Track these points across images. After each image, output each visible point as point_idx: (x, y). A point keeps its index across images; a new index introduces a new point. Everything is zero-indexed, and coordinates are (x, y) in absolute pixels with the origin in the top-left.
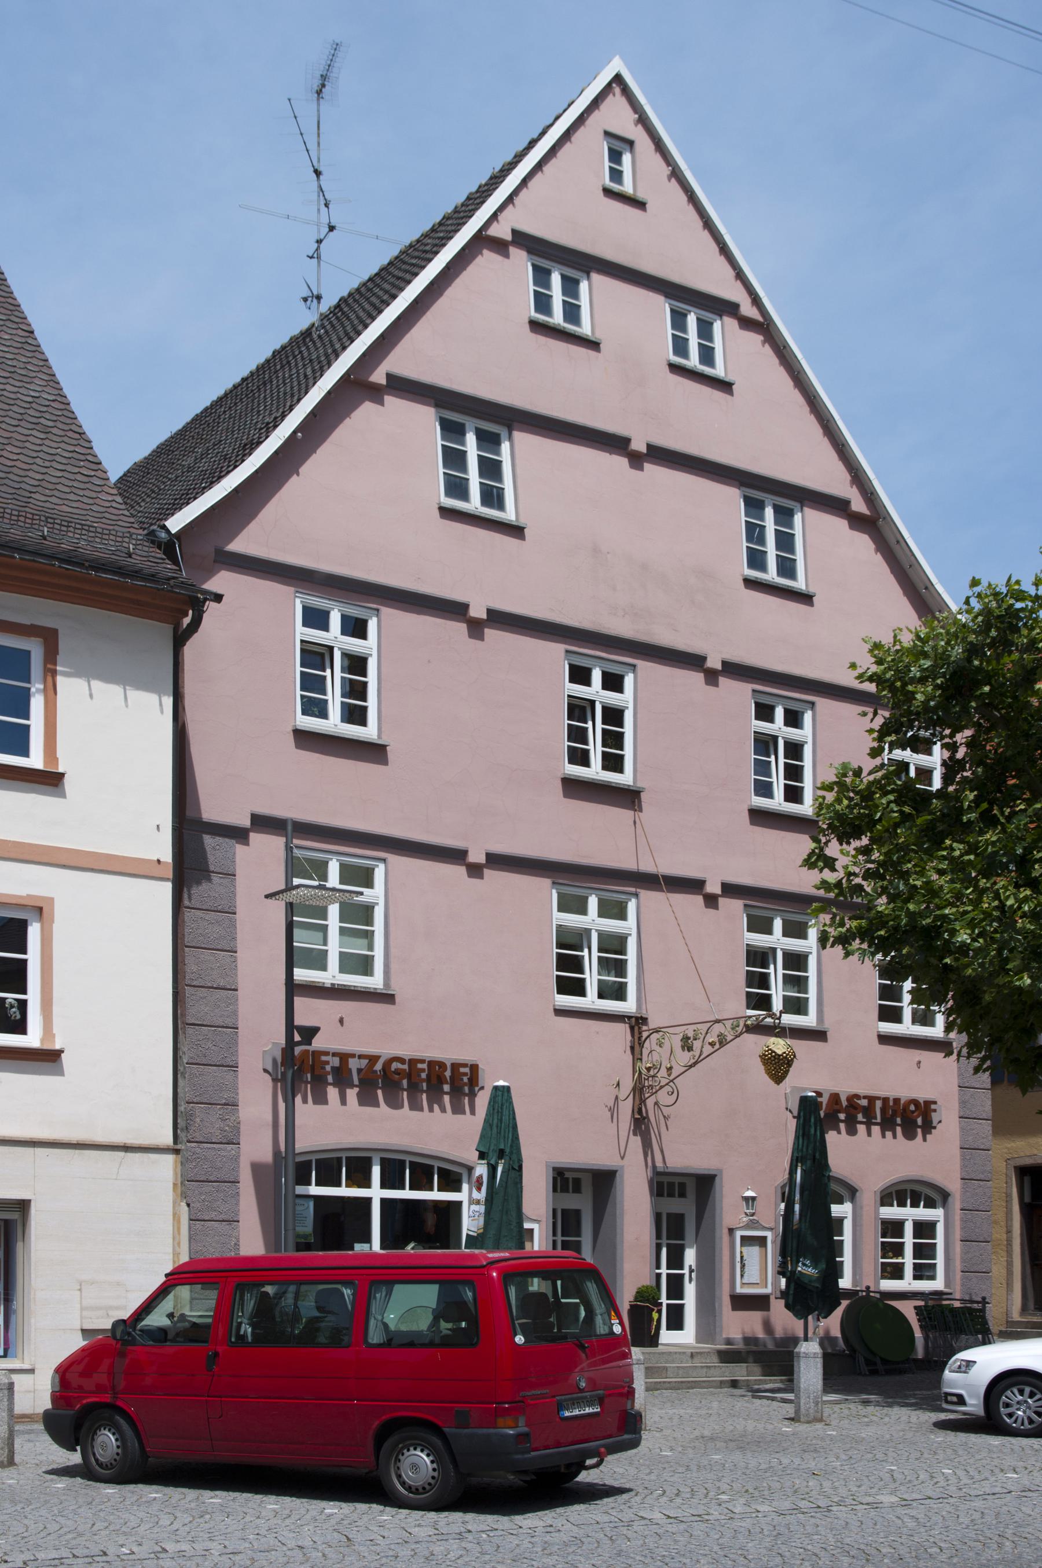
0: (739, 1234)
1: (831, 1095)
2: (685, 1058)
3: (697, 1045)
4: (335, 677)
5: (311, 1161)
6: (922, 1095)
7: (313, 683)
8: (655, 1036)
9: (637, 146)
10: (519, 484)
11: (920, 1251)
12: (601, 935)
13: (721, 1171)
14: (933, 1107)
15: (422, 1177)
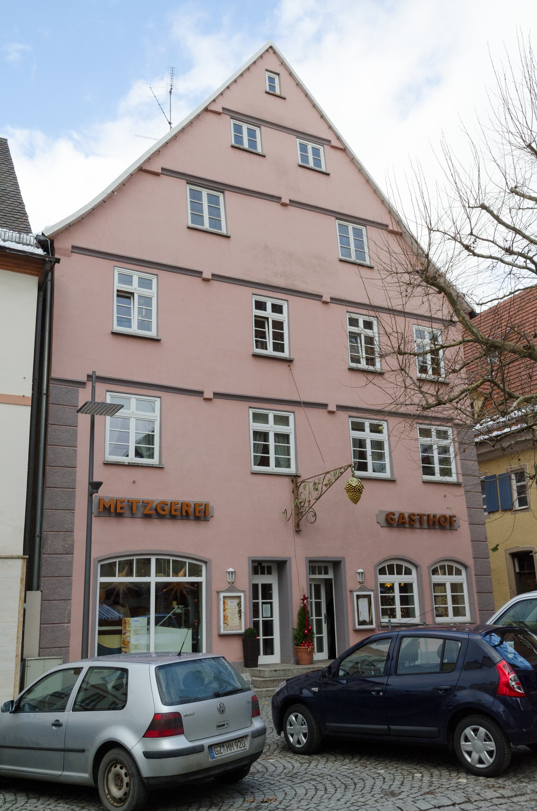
0: (355, 594)
1: (400, 514)
2: (315, 494)
3: (320, 486)
4: (269, 331)
5: (385, 566)
6: (448, 513)
7: (261, 335)
8: (303, 484)
9: (281, 75)
10: (228, 218)
11: (455, 600)
12: (372, 442)
13: (344, 558)
14: (454, 519)
15: (178, 568)
